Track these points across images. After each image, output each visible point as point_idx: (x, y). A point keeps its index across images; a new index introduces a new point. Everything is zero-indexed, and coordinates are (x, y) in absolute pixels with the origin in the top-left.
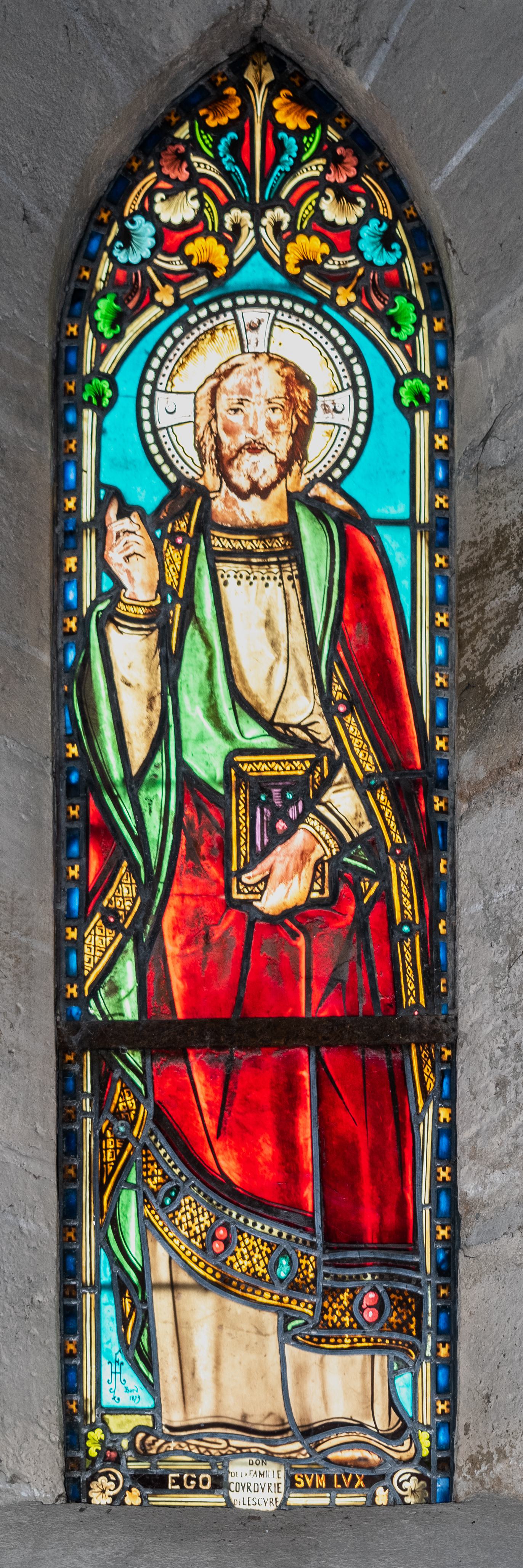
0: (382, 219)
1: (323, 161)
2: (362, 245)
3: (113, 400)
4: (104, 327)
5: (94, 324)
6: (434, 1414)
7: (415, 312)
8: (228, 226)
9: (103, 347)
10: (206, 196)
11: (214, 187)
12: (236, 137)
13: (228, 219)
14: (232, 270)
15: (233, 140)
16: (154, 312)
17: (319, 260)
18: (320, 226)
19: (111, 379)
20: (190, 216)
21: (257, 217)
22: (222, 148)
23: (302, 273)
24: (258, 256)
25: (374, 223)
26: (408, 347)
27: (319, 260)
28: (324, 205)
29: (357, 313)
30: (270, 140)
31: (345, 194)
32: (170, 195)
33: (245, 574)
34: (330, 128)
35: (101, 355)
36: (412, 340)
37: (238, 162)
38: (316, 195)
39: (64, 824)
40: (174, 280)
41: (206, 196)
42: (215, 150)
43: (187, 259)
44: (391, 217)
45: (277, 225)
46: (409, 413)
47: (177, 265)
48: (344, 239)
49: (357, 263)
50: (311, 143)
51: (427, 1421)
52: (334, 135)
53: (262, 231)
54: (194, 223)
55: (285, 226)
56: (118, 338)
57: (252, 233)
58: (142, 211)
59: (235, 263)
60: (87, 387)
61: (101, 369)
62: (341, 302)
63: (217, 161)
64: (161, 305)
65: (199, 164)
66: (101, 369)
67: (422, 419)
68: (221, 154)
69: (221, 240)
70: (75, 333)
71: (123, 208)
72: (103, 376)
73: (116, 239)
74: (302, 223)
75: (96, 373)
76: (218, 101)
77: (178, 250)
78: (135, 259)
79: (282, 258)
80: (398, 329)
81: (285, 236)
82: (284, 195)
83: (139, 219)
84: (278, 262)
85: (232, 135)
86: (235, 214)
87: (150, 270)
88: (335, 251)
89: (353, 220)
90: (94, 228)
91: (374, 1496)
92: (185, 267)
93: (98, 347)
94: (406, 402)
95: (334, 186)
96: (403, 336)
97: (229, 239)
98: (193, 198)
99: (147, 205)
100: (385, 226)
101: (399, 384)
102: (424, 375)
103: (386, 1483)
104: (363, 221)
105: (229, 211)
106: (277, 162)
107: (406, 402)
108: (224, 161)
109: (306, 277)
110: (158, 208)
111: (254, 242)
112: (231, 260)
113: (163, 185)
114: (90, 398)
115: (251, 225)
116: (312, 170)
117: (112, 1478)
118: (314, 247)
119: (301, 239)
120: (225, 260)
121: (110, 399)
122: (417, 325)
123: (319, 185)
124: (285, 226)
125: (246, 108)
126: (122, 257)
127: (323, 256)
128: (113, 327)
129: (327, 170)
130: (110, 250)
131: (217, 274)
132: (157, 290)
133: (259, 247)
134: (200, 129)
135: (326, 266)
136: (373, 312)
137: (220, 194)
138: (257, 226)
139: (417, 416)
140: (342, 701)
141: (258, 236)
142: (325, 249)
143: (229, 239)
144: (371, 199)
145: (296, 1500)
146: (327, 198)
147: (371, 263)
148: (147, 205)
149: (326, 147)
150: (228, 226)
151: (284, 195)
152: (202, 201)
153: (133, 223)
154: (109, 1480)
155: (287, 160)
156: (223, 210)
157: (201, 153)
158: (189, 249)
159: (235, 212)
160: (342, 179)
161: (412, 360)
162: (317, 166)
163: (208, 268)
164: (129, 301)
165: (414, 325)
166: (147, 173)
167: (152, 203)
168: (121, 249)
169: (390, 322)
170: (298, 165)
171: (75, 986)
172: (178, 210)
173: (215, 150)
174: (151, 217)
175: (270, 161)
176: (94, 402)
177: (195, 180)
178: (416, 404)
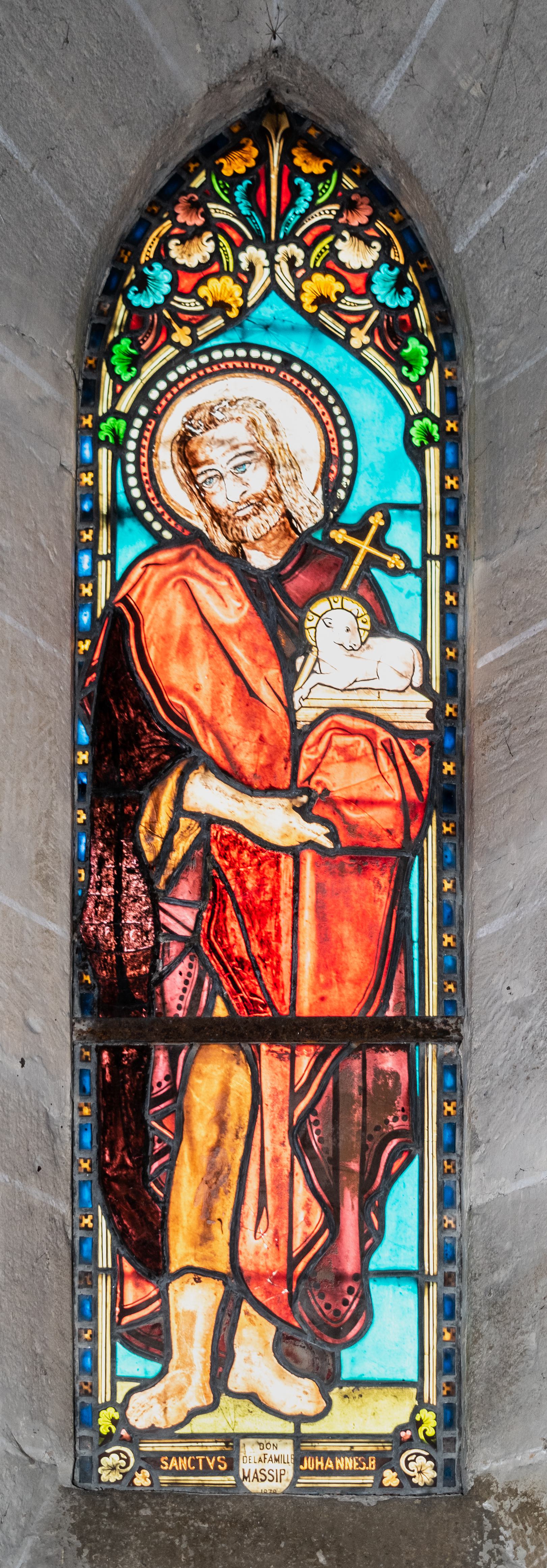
0: (393, 265)
1: (337, 207)
2: (375, 289)
5: (111, 369)
8: (244, 266)
9: (119, 388)
10: (221, 238)
16: (168, 353)
17: (334, 299)
22: (238, 194)
26: (418, 388)
27: (334, 299)
29: (371, 354)
30: (285, 187)
32: (184, 239)
33: (182, 1003)
34: (345, 176)
35: (117, 397)
36: (423, 379)
38: (330, 239)
39: (77, 1121)
41: (221, 238)
42: (231, 196)
43: (203, 301)
44: (402, 262)
45: (291, 261)
47: (191, 305)
49: (371, 306)
52: (349, 183)
54: (210, 264)
55: (299, 263)
56: (133, 380)
57: (267, 271)
59: (249, 305)
60: (103, 426)
63: (233, 205)
64: (177, 345)
67: (432, 455)
69: (237, 280)
71: (140, 254)
72: (118, 415)
73: (132, 283)
74: (316, 260)
78: (147, 304)
82: (298, 234)
83: (157, 266)
84: (292, 297)
85: (246, 182)
87: (165, 313)
88: (350, 292)
97: (244, 277)
98: (208, 240)
99: (162, 252)
100: (396, 271)
101: (409, 424)
102: (433, 415)
105: (244, 250)
106: (292, 205)
108: (241, 206)
110: (173, 254)
111: (269, 281)
114: (107, 437)
115: (267, 263)
116: (328, 212)
117: (413, 1457)
118: (330, 285)
119: (317, 277)
123: (333, 228)
124: (299, 263)
126: (138, 300)
129: (339, 214)
130: (125, 292)
132: (175, 331)
133: (273, 287)
134: (217, 181)
135: (340, 305)
137: (235, 236)
138: (273, 263)
139: (427, 452)
141: (273, 273)
143: (244, 277)
147: (384, 305)
149: (340, 194)
150: (244, 266)
151: (298, 234)
152: (217, 242)
153: (151, 269)
154: (121, 1458)
156: (237, 249)
157: (219, 201)
159: (251, 249)
161: (421, 396)
163: (221, 307)
164: (144, 342)
166: (163, 221)
167: (167, 250)
168: (136, 293)
170: (313, 206)
173: (231, 196)
175: (285, 199)
176: (111, 440)
177: (212, 225)
178: (426, 443)
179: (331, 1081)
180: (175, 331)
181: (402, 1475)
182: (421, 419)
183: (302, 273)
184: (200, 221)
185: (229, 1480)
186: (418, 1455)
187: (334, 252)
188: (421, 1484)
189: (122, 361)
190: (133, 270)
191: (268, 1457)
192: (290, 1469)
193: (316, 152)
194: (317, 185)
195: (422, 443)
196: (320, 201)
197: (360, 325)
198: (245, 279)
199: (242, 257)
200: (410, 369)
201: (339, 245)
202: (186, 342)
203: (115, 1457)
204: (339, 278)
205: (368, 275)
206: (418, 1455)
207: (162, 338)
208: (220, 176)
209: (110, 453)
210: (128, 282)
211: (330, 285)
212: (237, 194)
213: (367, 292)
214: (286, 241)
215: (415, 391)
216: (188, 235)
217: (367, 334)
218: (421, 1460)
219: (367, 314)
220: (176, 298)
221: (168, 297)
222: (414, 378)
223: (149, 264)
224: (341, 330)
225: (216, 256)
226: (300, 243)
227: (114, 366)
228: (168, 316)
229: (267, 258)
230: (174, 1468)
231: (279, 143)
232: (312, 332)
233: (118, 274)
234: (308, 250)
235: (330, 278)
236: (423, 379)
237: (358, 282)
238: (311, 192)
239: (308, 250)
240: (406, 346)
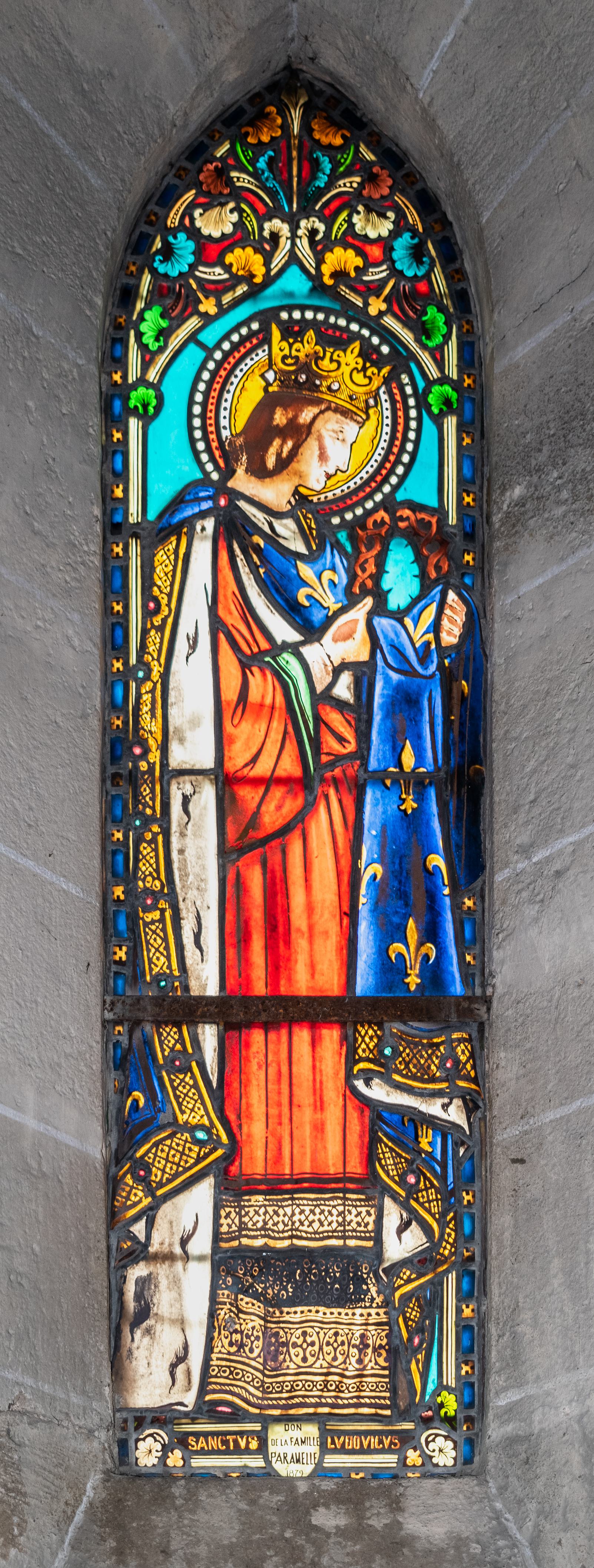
3: (158, 408)
4: (149, 339)
5: (139, 335)
6: (458, 1377)
8: (266, 234)
10: (243, 206)
11: (252, 198)
14: (269, 280)
15: (270, 158)
18: (353, 240)
19: (156, 387)
20: (229, 229)
24: (294, 270)
25: (407, 236)
28: (355, 219)
29: (389, 321)
31: (376, 209)
34: (362, 145)
35: (146, 365)
36: (440, 348)
38: (344, 215)
40: (216, 289)
43: (228, 268)
45: (313, 232)
46: (438, 420)
47: (217, 274)
51: (452, 1383)
53: (298, 241)
56: (161, 350)
57: (289, 242)
58: (181, 227)
59: (272, 273)
62: (373, 311)
65: (238, 178)
72: (149, 385)
79: (318, 268)
80: (428, 337)
81: (319, 248)
83: (182, 236)
84: (313, 271)
89: (385, 233)
91: (406, 1458)
92: (226, 276)
94: (436, 410)
98: (231, 211)
99: (187, 221)
102: (452, 379)
103: (414, 1443)
104: (395, 234)
110: (198, 224)
112: (268, 270)
113: (202, 200)
115: (289, 235)
116: (348, 184)
118: (348, 259)
119: (338, 251)
120: (263, 270)
121: (154, 408)
124: (319, 237)
125: (286, 127)
127: (357, 269)
128: (157, 339)
132: (201, 302)
133: (293, 258)
135: (358, 179)
138: (294, 236)
141: (294, 244)
142: (359, 262)
144: (401, 216)
145: (333, 1461)
146: (358, 213)
148: (187, 221)
150: (266, 234)
152: (241, 211)
157: (243, 170)
158: (229, 258)
161: (440, 363)
162: (351, 183)
165: (444, 336)
167: (192, 220)
168: (161, 262)
169: (422, 331)
172: (216, 223)
174: (194, 233)
176: (141, 410)
180: (201, 302)
181: (423, 1454)
185: (256, 1462)
186: (437, 1435)
187: (351, 225)
188: (441, 1464)
191: (294, 1440)
192: (315, 1449)
193: (334, 124)
195: (441, 410)
198: (267, 247)
199: (267, 226)
203: (150, 1440)
204: (360, 252)
205: (386, 244)
206: (437, 1435)
207: (189, 310)
208: (246, 145)
209: (140, 424)
210: (154, 249)
211: (348, 259)
217: (384, 301)
218: (440, 1441)
219: (384, 282)
220: (201, 268)
221: (192, 267)
222: (430, 344)
223: (174, 232)
225: (239, 225)
228: (194, 286)
230: (203, 1448)
231: (299, 121)
233: (145, 240)
234: (329, 223)
235: (351, 253)
236: (440, 348)
237: (376, 252)
239: (329, 223)
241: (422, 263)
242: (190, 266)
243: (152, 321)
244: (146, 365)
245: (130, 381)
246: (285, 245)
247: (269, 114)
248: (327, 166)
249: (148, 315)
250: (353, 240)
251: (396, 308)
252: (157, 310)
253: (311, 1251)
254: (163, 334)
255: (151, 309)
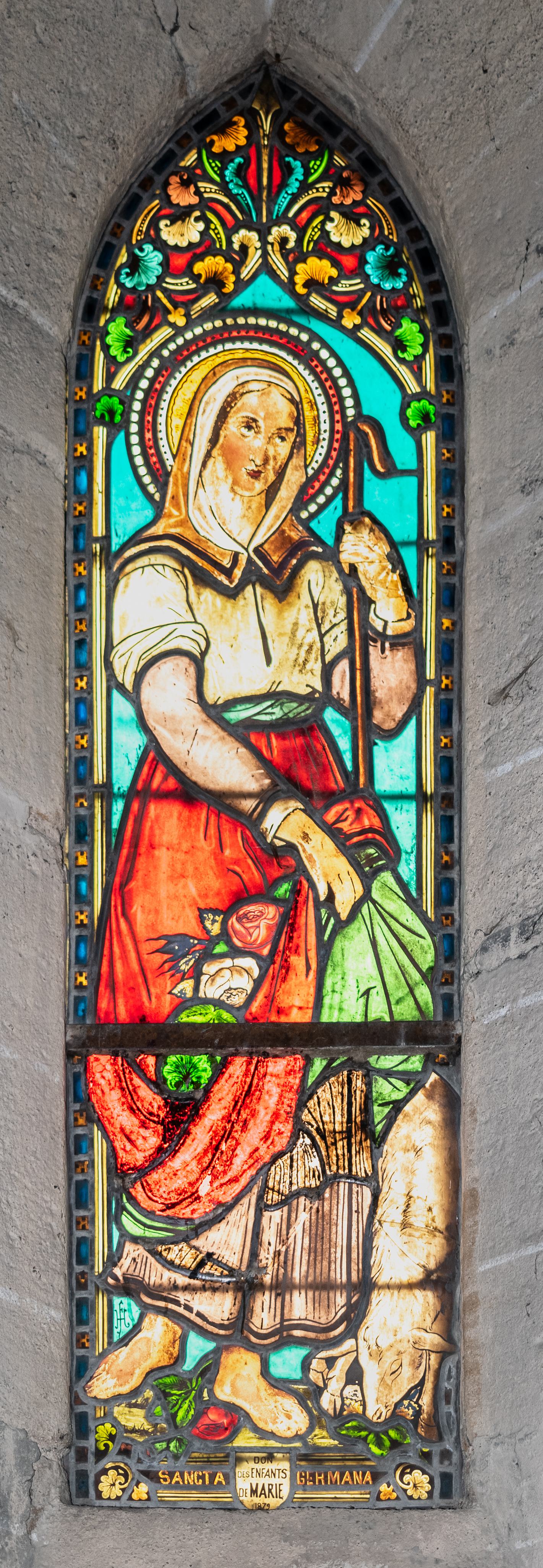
4: (116, 351)
5: (106, 348)
7: (421, 331)
8: (236, 246)
12: (242, 160)
13: (236, 239)
14: (241, 285)
15: (240, 165)
16: (165, 332)
18: (326, 248)
20: (196, 238)
21: (263, 233)
23: (308, 295)
25: (380, 248)
29: (366, 334)
31: (351, 216)
35: (110, 377)
37: (246, 186)
38: (321, 218)
40: (184, 301)
42: (222, 176)
43: (196, 278)
45: (284, 241)
46: (416, 433)
47: (184, 284)
48: (349, 261)
49: (362, 286)
50: (316, 171)
53: (269, 247)
55: (291, 244)
56: (129, 360)
61: (113, 386)
63: (224, 187)
64: (173, 325)
66: (113, 386)
68: (227, 179)
70: (85, 453)
75: (108, 391)
76: (224, 129)
77: (188, 271)
82: (291, 214)
83: (148, 247)
86: (242, 235)
87: (159, 294)
90: (103, 257)
92: (194, 286)
93: (108, 370)
94: (413, 423)
95: (339, 208)
96: (408, 356)
107: (413, 423)
108: (231, 186)
109: (311, 299)
110: (164, 235)
111: (260, 261)
115: (258, 245)
118: (319, 268)
119: (313, 261)
122: (425, 346)
124: (291, 244)
127: (331, 278)
129: (332, 193)
130: (118, 274)
131: (225, 291)
135: (330, 184)
136: (379, 331)
137: (228, 217)
139: (424, 437)
140: (116, 1278)
141: (265, 255)
142: (334, 273)
146: (332, 220)
150: (236, 246)
151: (291, 214)
152: (208, 222)
155: (293, 186)
156: (230, 232)
157: (212, 181)
159: (243, 232)
160: (348, 201)
161: (418, 375)
167: (158, 230)
168: (128, 275)
169: (399, 345)
170: (305, 187)
171: (85, 445)
172: (183, 234)
173: (222, 176)
174: (160, 245)
175: (277, 180)
176: (107, 418)
177: (205, 204)
179: (326, 938)
182: (419, 401)
183: (295, 257)
184: (195, 200)
187: (325, 234)
189: (118, 340)
190: (124, 250)
191: (265, 1471)
194: (309, 162)
196: (311, 179)
197: (352, 306)
200: (128, 275)
201: (329, 226)
202: (181, 322)
204: (335, 264)
205: (359, 252)
208: (212, 156)
212: (227, 173)
213: (358, 270)
214: (278, 222)
215: (412, 372)
216: (180, 215)
220: (168, 280)
221: (160, 279)
224: (333, 311)
226: (293, 224)
227: (108, 347)
229: (260, 240)
232: (289, 604)
235: (326, 263)
237: (349, 262)
238: (301, 170)
239: (301, 232)
240: (400, 326)
241: (399, 275)
242: (158, 277)
243: (118, 329)
244: (110, 377)
245: (95, 390)
246: (254, 260)
247: (235, 123)
248: (299, 173)
249: (111, 327)
250: (326, 248)
251: (371, 321)
252: (121, 321)
253: (290, 352)
254: (131, 344)
255: (114, 321)
